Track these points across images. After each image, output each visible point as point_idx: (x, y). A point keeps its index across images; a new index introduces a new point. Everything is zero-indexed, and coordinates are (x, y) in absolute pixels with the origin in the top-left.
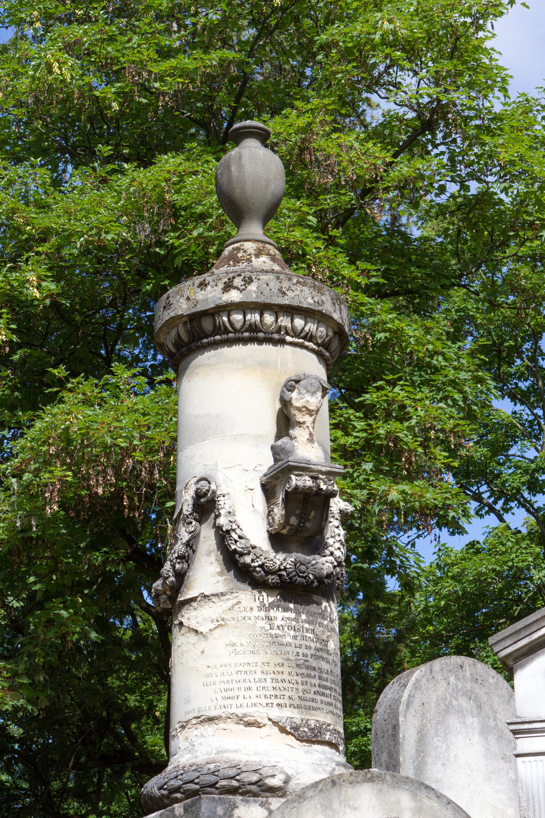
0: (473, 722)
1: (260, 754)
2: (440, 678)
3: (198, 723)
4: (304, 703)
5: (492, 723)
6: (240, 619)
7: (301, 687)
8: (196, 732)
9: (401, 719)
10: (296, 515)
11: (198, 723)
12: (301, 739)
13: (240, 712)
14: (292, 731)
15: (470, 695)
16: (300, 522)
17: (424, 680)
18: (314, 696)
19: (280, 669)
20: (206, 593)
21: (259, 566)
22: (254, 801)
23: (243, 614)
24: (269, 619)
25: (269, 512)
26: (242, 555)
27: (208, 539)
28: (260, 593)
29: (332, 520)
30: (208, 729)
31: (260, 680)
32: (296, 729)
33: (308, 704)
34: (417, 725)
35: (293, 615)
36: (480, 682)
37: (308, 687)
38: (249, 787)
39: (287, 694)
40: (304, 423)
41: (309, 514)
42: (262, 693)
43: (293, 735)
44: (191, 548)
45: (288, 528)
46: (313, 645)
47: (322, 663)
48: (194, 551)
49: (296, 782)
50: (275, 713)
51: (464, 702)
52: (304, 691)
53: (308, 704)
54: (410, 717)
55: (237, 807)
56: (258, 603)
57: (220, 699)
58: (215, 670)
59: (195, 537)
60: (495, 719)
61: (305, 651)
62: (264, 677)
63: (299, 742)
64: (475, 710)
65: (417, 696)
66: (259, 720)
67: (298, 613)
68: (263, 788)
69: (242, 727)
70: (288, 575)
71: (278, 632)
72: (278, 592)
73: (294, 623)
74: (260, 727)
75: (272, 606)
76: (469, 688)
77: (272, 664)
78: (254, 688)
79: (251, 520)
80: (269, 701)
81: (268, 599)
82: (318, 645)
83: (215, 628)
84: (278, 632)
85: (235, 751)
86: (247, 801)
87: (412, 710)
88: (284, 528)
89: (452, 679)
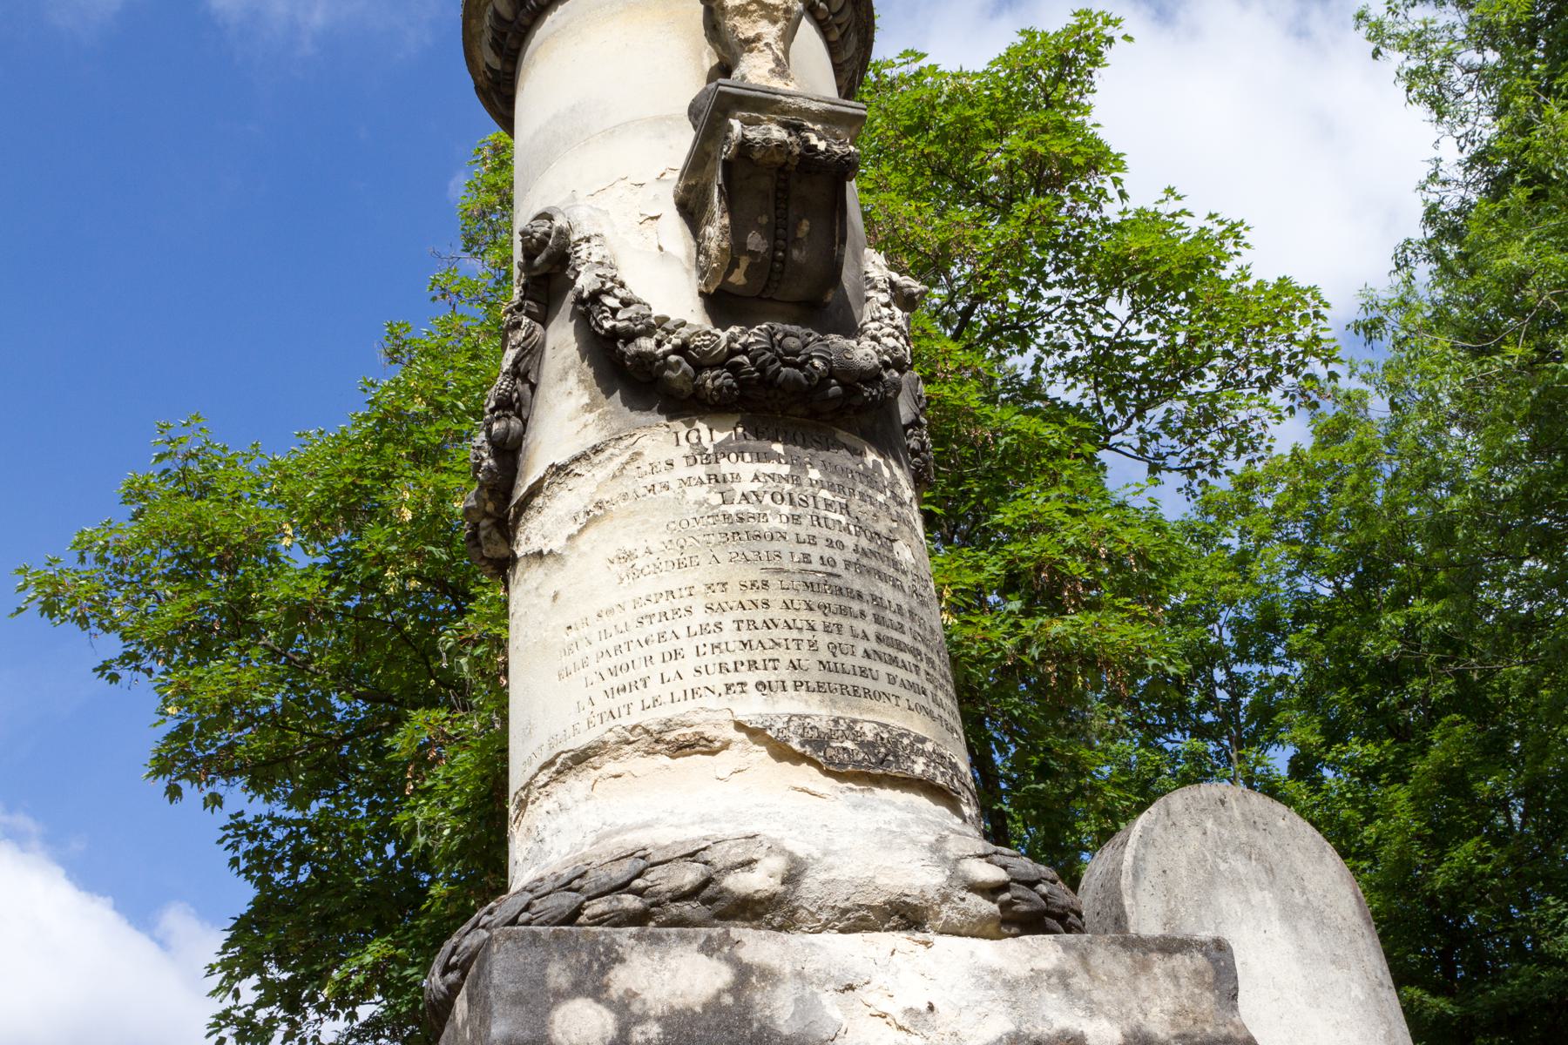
0: (1264, 898)
1: (715, 820)
2: (1187, 823)
3: (552, 780)
4: (836, 678)
5: (1298, 899)
6: (642, 491)
7: (823, 639)
8: (548, 804)
9: (1127, 902)
10: (760, 228)
11: (552, 780)
12: (838, 771)
13: (652, 719)
14: (808, 750)
15: (1249, 851)
16: (776, 249)
17: (1158, 830)
18: (866, 663)
19: (760, 596)
20: (559, 461)
21: (677, 350)
22: (682, 937)
23: (649, 480)
24: (715, 479)
25: (699, 245)
26: (630, 336)
27: (561, 338)
28: (690, 424)
29: (871, 293)
30: (577, 785)
31: (703, 629)
32: (820, 742)
33: (849, 680)
34: (1159, 911)
35: (785, 470)
36: (1261, 827)
37: (846, 639)
38: (674, 909)
39: (785, 656)
40: (758, 38)
41: (796, 226)
42: (711, 659)
43: (812, 762)
44: (525, 379)
45: (744, 262)
46: (850, 541)
47: (881, 585)
48: (533, 387)
49: (824, 876)
50: (753, 708)
51: (1239, 864)
52: (834, 648)
53: (849, 680)
54: (1143, 897)
55: (621, 960)
56: (685, 448)
57: (600, 699)
58: (585, 630)
59: (532, 353)
60: (1303, 891)
61: (828, 553)
62: (713, 618)
63: (832, 781)
64: (1263, 877)
65: (1150, 858)
66: (710, 732)
67: (798, 464)
68: (719, 906)
69: (663, 760)
70: (753, 361)
71: (744, 507)
72: (738, 418)
73: (788, 487)
74: (713, 753)
75: (722, 450)
76: (1244, 839)
77: (734, 586)
78: (689, 651)
79: (658, 272)
80: (733, 678)
81: (708, 435)
82: (864, 543)
83: (580, 531)
84: (744, 507)
85: (646, 825)
86: (657, 940)
87: (1146, 884)
88: (734, 264)
89: (1209, 824)
